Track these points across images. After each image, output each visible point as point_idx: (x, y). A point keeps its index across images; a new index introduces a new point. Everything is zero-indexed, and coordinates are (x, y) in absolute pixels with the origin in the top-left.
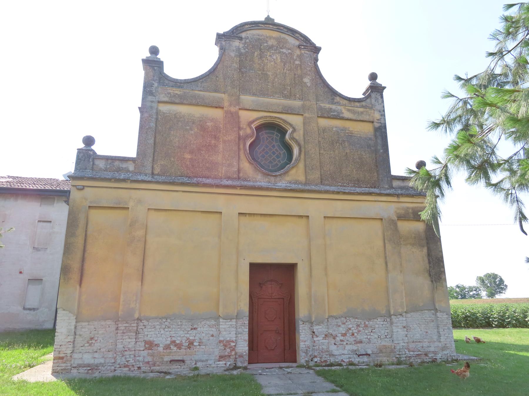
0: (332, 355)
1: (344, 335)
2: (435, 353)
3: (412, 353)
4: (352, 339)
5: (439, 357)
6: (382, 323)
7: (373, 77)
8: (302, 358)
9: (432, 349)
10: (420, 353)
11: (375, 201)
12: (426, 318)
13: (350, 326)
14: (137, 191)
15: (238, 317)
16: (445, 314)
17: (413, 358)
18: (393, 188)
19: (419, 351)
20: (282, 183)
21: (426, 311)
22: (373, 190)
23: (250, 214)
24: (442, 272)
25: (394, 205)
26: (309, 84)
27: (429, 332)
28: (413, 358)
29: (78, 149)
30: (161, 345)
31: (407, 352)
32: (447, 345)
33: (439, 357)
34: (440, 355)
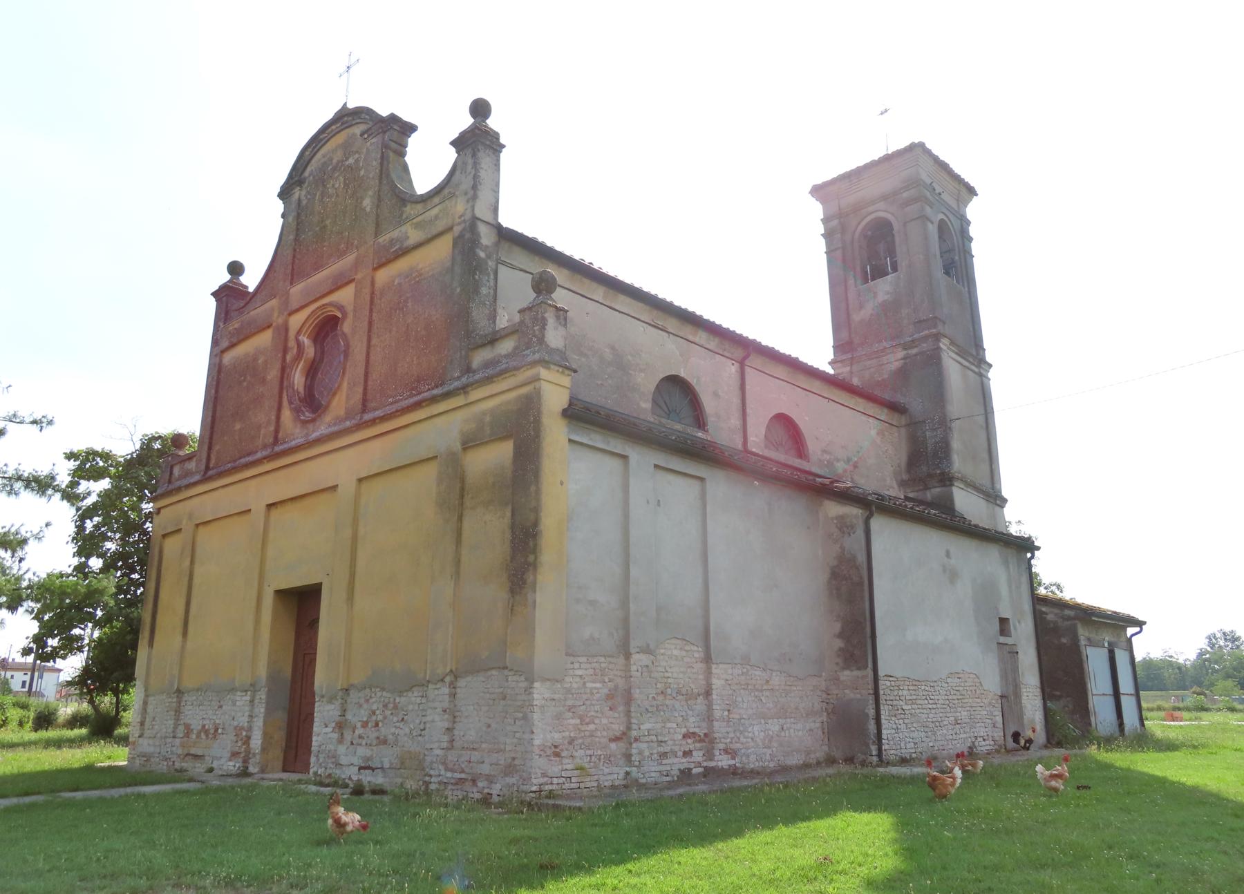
0: (338, 765)
1: (365, 725)
2: (490, 779)
3: (449, 774)
4: (372, 734)
5: (496, 789)
6: (418, 700)
7: (480, 109)
8: (316, 766)
9: (485, 769)
10: (463, 776)
11: (454, 409)
12: (491, 690)
13: (375, 707)
14: (186, 502)
15: (253, 687)
16: (522, 678)
17: (450, 787)
18: (474, 372)
19: (463, 771)
20: (322, 429)
21: (494, 672)
22: (435, 392)
23: (292, 499)
24: (529, 564)
25: (459, 416)
26: (368, 209)
27: (493, 725)
28: (450, 787)
29: (819, 191)
30: (32, 709)
31: (443, 772)
32: (516, 762)
33: (496, 789)
34: (498, 786)
